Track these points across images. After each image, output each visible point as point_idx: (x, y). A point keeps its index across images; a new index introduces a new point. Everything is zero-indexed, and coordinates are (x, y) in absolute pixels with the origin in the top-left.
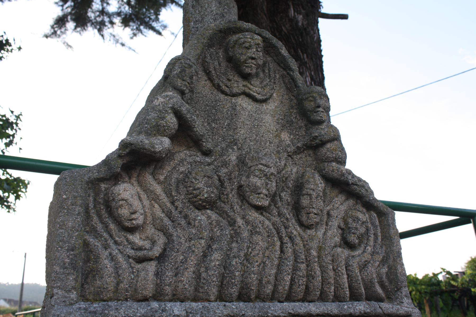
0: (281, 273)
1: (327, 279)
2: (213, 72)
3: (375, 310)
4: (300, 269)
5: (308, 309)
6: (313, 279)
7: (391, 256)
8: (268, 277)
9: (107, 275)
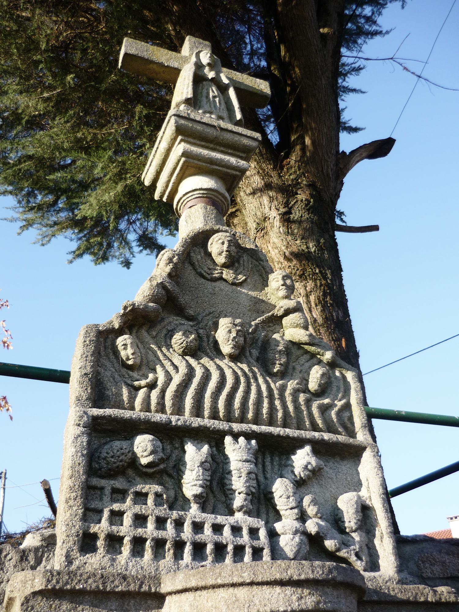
2: (196, 263)
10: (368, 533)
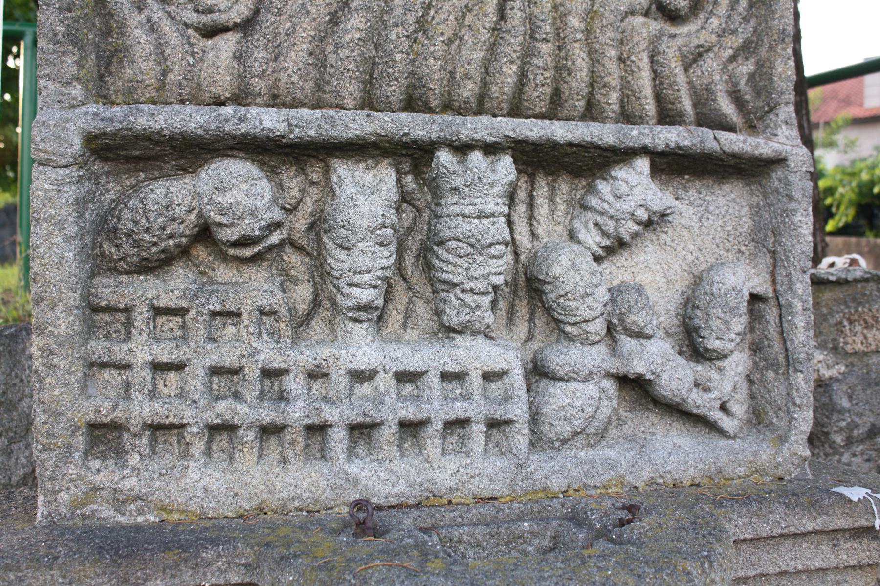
0: (496, 60)
1: (602, 78)
3: (701, 142)
4: (539, 53)
5: (548, 131)
6: (569, 74)
7: (765, 40)
8: (466, 65)
9: (141, 57)
10: (755, 352)
